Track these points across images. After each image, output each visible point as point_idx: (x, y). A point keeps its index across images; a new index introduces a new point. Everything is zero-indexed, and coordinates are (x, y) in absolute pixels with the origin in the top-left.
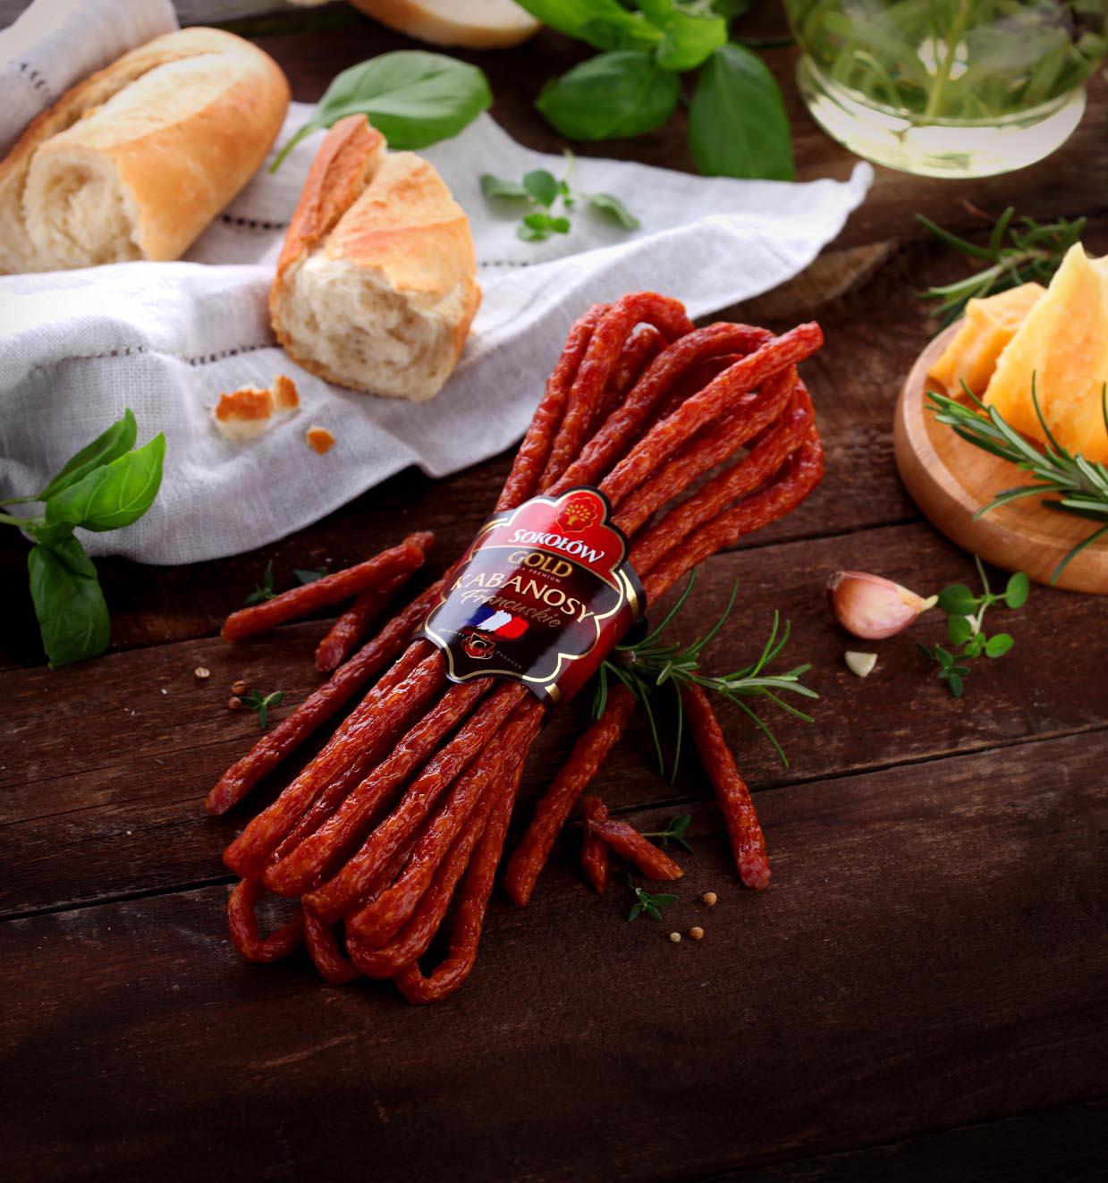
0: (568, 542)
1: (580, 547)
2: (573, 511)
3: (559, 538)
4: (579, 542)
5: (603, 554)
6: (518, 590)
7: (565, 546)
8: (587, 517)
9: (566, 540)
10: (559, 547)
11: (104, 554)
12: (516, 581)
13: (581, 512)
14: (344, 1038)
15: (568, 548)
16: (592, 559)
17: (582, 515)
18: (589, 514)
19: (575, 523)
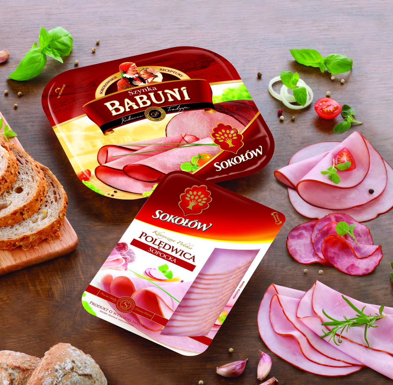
0: (189, 221)
1: (197, 223)
2: (192, 197)
3: (183, 220)
5: (211, 225)
6: (135, 107)
7: (187, 224)
8: (204, 202)
9: (187, 220)
10: (184, 225)
11: (13, 266)
12: (128, 104)
13: (199, 198)
14: (344, 239)
15: (189, 225)
17: (199, 200)
18: (205, 199)
19: (193, 207)
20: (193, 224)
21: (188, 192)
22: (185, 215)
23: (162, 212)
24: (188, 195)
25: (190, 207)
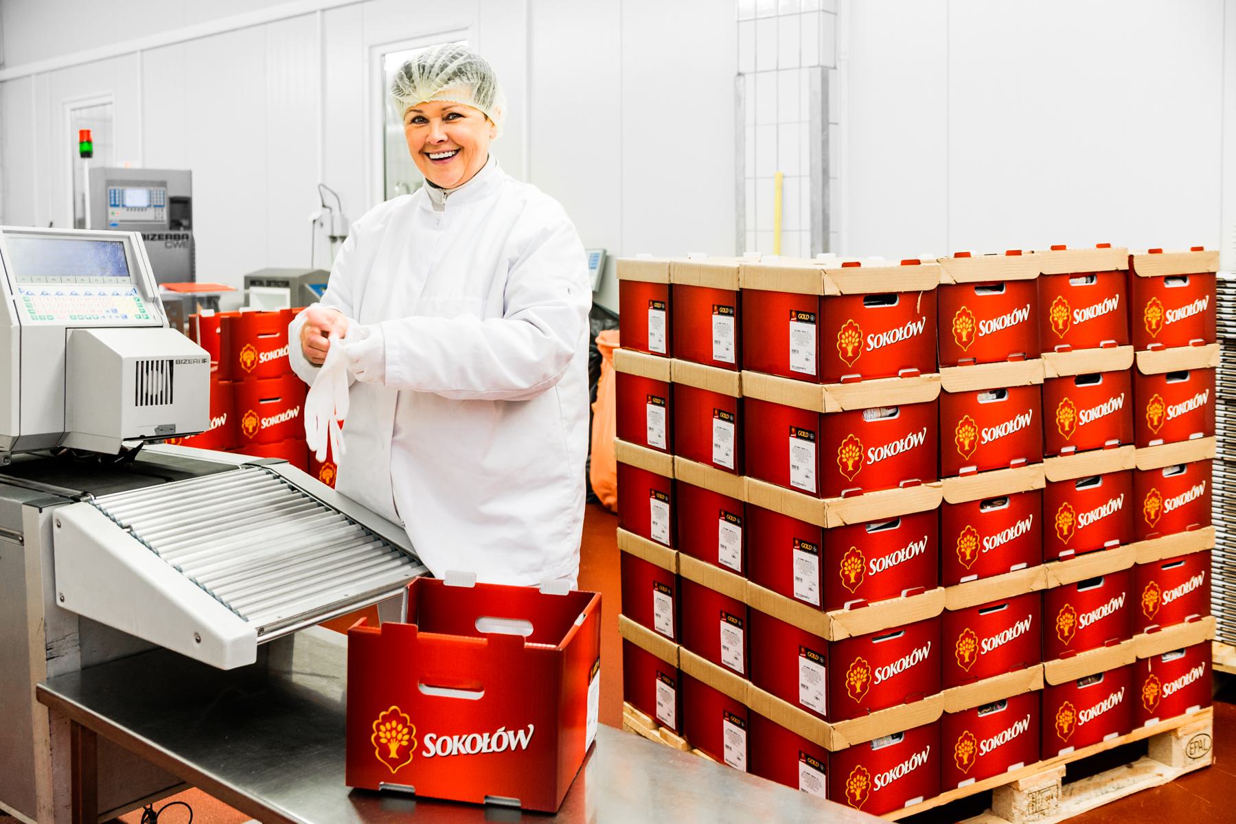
0: (490, 737)
4: (500, 731)
5: (531, 727)
7: (489, 746)
8: (407, 737)
10: (485, 750)
13: (398, 733)
16: (524, 745)
17: (400, 736)
18: (406, 730)
19: (398, 752)
20: (500, 739)
21: (379, 730)
22: (395, 710)
23: (434, 736)
24: (381, 734)
25: (393, 755)
